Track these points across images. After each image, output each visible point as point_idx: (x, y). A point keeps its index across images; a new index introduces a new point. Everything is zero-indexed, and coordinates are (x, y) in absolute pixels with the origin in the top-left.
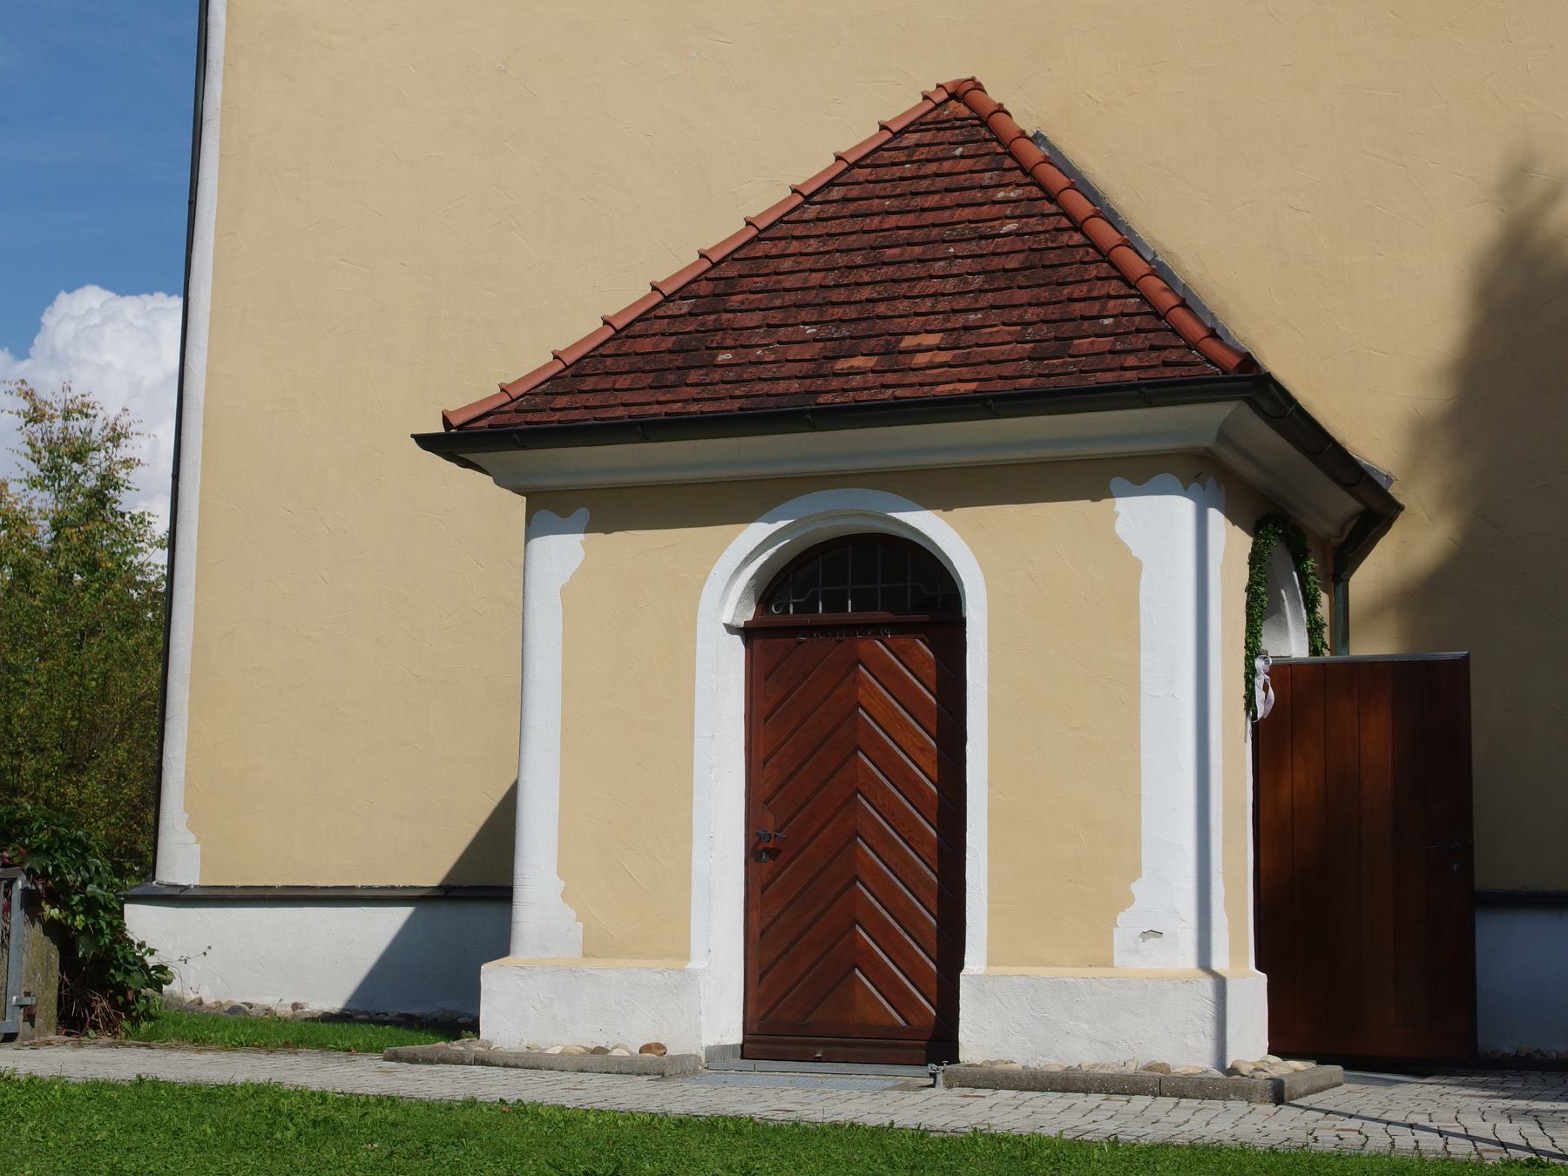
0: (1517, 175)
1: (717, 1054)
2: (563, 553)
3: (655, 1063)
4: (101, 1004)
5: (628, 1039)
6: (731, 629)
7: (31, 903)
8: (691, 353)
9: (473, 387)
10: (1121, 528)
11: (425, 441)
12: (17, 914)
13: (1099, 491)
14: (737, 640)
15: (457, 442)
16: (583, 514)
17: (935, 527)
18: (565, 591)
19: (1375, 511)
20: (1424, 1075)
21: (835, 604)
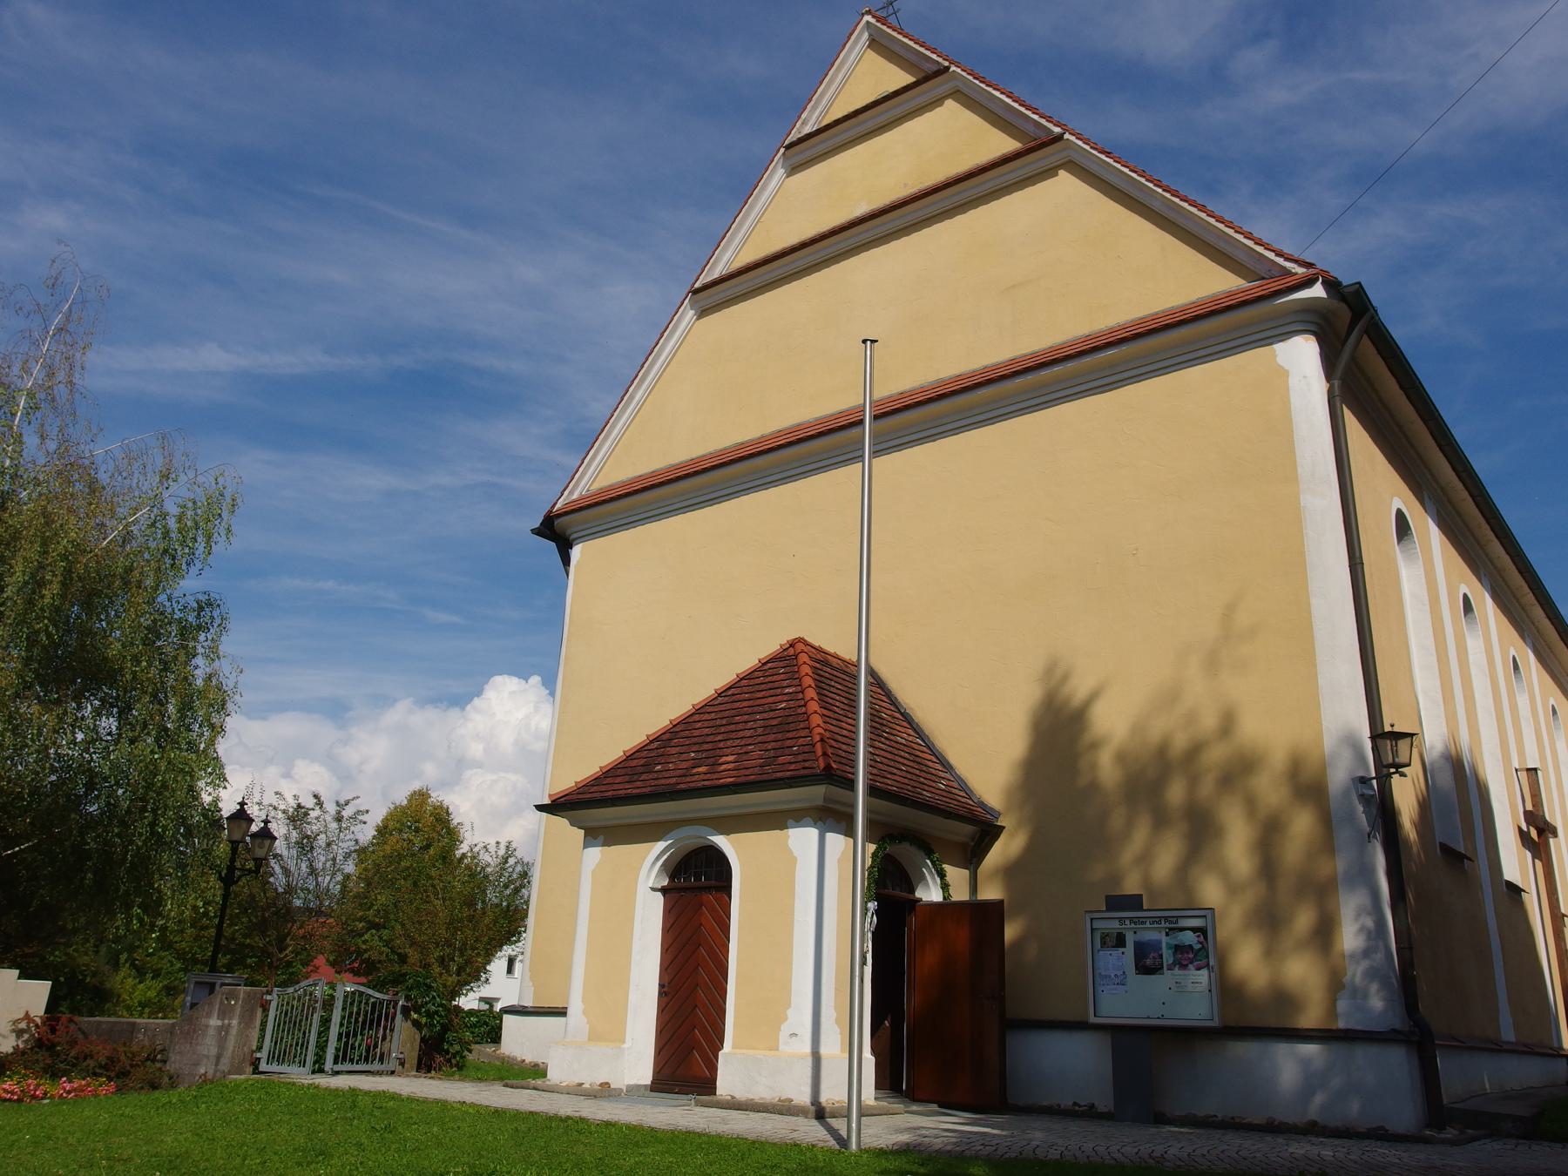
0: (1049, 671)
1: (633, 1090)
2: (595, 854)
3: (604, 1091)
4: (439, 1059)
5: (591, 1079)
6: (653, 889)
7: (406, 1012)
8: (648, 767)
9: (568, 780)
10: (791, 843)
11: (540, 808)
12: (399, 1016)
13: (783, 826)
14: (659, 894)
15: (556, 806)
16: (601, 838)
17: (721, 841)
18: (593, 872)
19: (986, 830)
20: (683, 1092)
21: (698, 879)
